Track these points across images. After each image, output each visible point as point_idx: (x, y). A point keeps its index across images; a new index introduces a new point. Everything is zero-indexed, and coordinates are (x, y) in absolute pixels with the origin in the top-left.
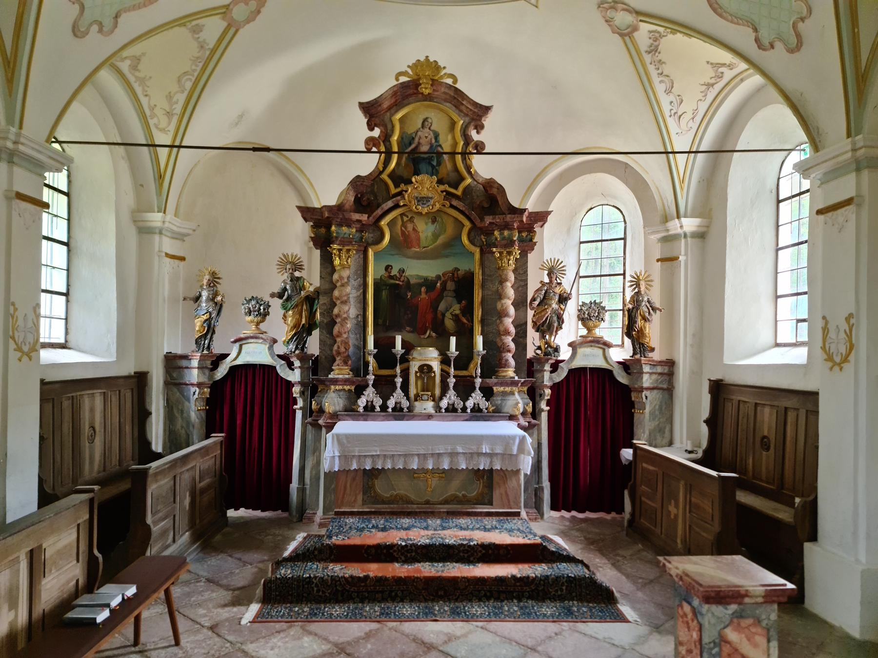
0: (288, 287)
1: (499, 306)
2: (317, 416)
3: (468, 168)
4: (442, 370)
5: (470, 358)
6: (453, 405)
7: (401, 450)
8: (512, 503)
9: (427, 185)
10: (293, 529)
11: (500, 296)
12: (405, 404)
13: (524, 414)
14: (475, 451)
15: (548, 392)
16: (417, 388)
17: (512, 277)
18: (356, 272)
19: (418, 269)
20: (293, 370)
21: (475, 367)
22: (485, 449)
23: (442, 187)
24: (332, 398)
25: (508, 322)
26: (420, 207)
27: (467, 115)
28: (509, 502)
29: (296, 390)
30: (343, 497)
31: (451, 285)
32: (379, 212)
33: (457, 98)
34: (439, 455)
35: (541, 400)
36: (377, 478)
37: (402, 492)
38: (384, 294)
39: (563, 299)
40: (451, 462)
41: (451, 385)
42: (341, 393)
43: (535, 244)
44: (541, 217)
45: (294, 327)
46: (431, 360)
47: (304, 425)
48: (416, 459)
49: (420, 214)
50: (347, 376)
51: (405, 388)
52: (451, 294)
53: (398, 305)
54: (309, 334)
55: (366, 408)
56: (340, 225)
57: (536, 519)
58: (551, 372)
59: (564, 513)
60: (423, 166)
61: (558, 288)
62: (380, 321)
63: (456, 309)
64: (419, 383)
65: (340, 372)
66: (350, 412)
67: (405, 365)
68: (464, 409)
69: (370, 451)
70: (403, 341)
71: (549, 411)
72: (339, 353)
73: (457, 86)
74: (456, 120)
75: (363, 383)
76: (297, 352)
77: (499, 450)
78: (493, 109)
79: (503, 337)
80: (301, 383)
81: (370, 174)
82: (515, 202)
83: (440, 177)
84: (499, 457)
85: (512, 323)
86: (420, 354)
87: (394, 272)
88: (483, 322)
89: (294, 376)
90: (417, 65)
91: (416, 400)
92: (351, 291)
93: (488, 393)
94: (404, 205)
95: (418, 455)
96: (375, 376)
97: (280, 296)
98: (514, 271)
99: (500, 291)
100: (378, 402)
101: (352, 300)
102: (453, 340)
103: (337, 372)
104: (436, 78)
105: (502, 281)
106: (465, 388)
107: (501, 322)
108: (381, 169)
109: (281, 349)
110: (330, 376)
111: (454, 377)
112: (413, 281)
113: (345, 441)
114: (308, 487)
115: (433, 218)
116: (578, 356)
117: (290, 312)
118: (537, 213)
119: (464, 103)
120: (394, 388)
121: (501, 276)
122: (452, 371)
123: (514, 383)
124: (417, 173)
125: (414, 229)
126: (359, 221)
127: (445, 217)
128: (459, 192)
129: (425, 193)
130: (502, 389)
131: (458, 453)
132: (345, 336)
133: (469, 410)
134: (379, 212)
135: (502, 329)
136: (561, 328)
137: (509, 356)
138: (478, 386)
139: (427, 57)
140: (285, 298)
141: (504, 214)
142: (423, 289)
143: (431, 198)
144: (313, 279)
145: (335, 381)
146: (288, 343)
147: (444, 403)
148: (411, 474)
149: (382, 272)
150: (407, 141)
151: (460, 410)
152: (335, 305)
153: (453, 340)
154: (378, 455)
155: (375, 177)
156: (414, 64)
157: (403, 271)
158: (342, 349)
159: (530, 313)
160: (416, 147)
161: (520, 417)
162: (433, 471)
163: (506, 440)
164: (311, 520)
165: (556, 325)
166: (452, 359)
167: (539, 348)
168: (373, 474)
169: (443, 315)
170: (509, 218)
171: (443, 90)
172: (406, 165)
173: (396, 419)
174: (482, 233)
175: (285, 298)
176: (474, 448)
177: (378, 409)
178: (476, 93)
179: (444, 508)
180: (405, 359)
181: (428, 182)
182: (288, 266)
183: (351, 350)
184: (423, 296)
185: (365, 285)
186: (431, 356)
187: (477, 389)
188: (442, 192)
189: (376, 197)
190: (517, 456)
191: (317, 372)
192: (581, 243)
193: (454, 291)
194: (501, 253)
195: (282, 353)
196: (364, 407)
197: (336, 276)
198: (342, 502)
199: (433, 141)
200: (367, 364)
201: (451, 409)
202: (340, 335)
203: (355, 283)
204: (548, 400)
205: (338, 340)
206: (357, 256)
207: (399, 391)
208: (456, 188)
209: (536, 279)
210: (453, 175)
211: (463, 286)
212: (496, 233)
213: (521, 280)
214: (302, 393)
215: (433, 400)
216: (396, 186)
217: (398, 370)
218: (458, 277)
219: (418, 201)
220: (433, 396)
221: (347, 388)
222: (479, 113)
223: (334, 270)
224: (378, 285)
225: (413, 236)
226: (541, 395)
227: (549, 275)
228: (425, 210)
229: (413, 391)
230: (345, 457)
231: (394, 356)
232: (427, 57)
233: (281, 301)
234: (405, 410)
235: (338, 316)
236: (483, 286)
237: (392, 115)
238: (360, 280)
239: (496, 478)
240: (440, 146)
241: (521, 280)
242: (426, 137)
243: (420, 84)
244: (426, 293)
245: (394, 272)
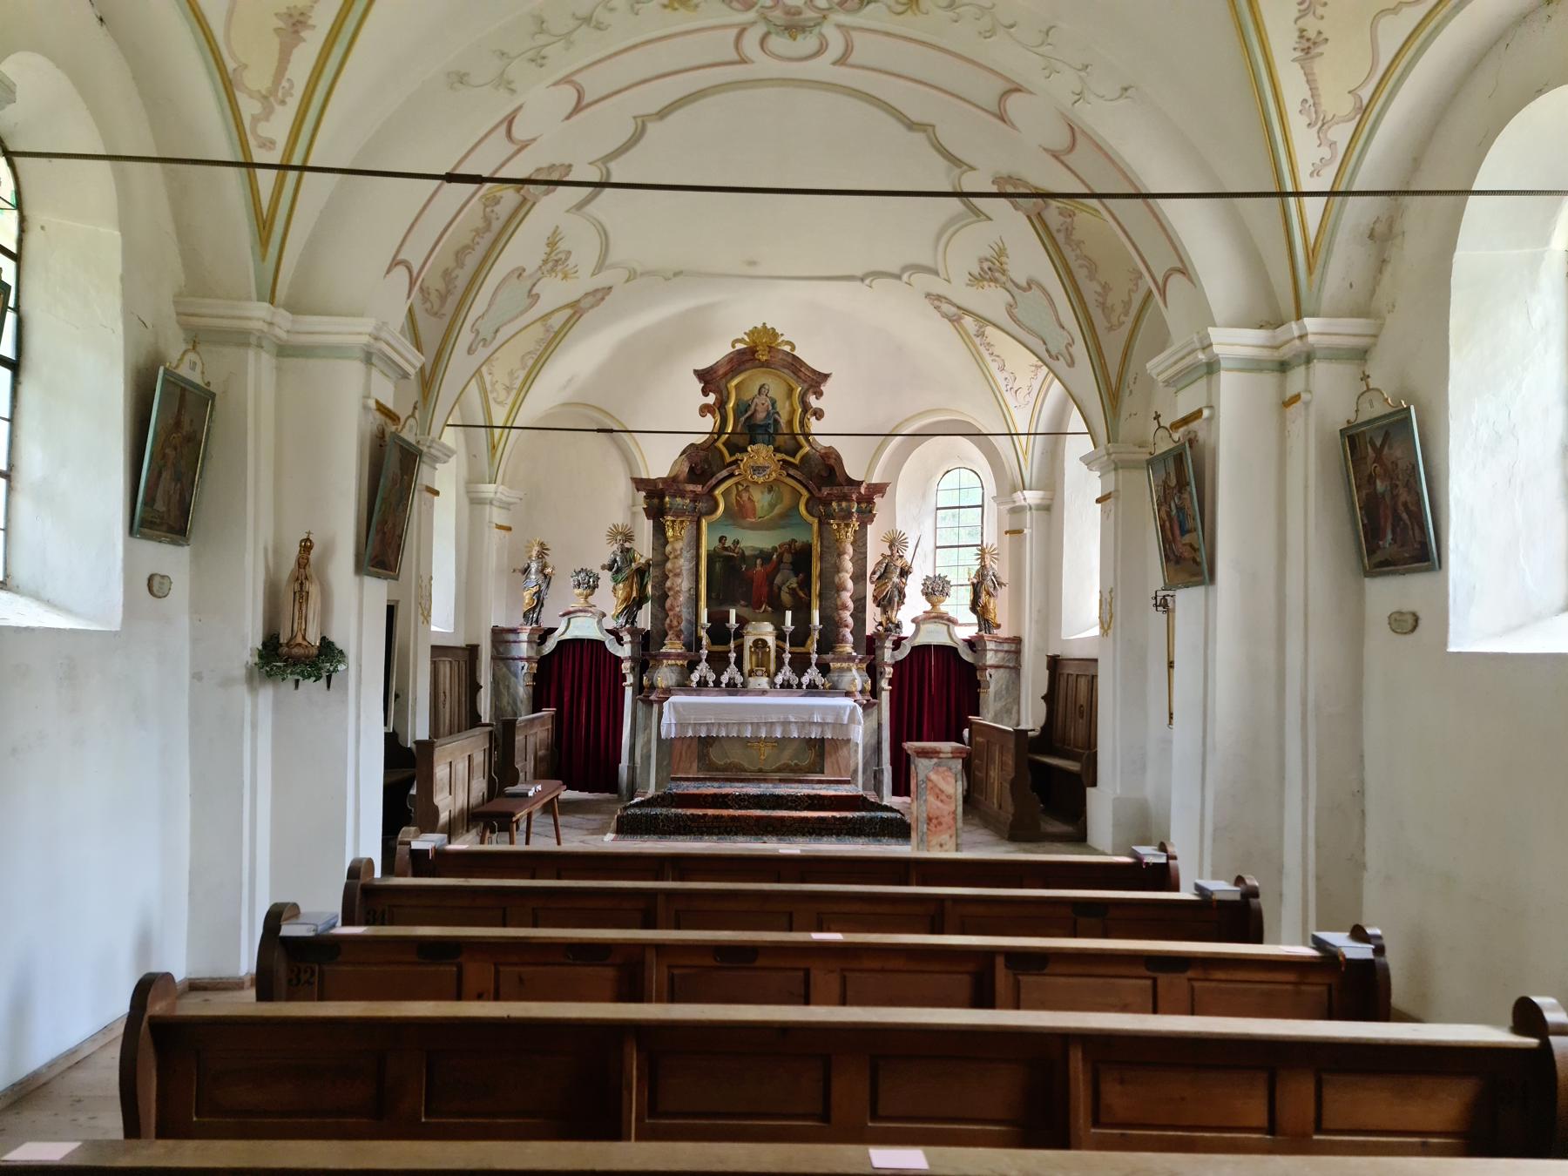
5: (808, 633)
7: (734, 718)
11: (838, 569)
12: (739, 679)
13: (862, 692)
15: (889, 670)
17: (850, 549)
19: (753, 541)
22: (817, 718)
25: (846, 597)
29: (626, 667)
31: (787, 558)
32: (713, 481)
33: (795, 365)
34: (772, 723)
39: (905, 573)
44: (880, 489)
51: (739, 663)
53: (731, 578)
54: (640, 608)
55: (698, 683)
56: (674, 496)
63: (793, 582)
65: (673, 646)
66: (683, 686)
68: (800, 685)
72: (671, 627)
77: (830, 720)
87: (728, 543)
88: (821, 596)
89: (624, 651)
90: (753, 333)
92: (684, 564)
93: (824, 669)
100: (711, 677)
102: (789, 614)
105: (840, 554)
109: (610, 623)
112: (747, 553)
123: (850, 659)
128: (796, 461)
129: (761, 462)
134: (713, 481)
137: (847, 632)
144: (644, 548)
145: (668, 656)
147: (779, 679)
153: (789, 614)
155: (709, 447)
168: (707, 742)
170: (846, 489)
176: (806, 718)
180: (739, 634)
183: (683, 625)
184: (759, 568)
185: (698, 557)
191: (648, 648)
197: (668, 548)
208: (794, 456)
209: (875, 552)
211: (800, 558)
216: (731, 455)
217: (732, 645)
220: (768, 672)
223: (666, 542)
225: (749, 505)
229: (747, 667)
230: (681, 725)
245: (728, 543)
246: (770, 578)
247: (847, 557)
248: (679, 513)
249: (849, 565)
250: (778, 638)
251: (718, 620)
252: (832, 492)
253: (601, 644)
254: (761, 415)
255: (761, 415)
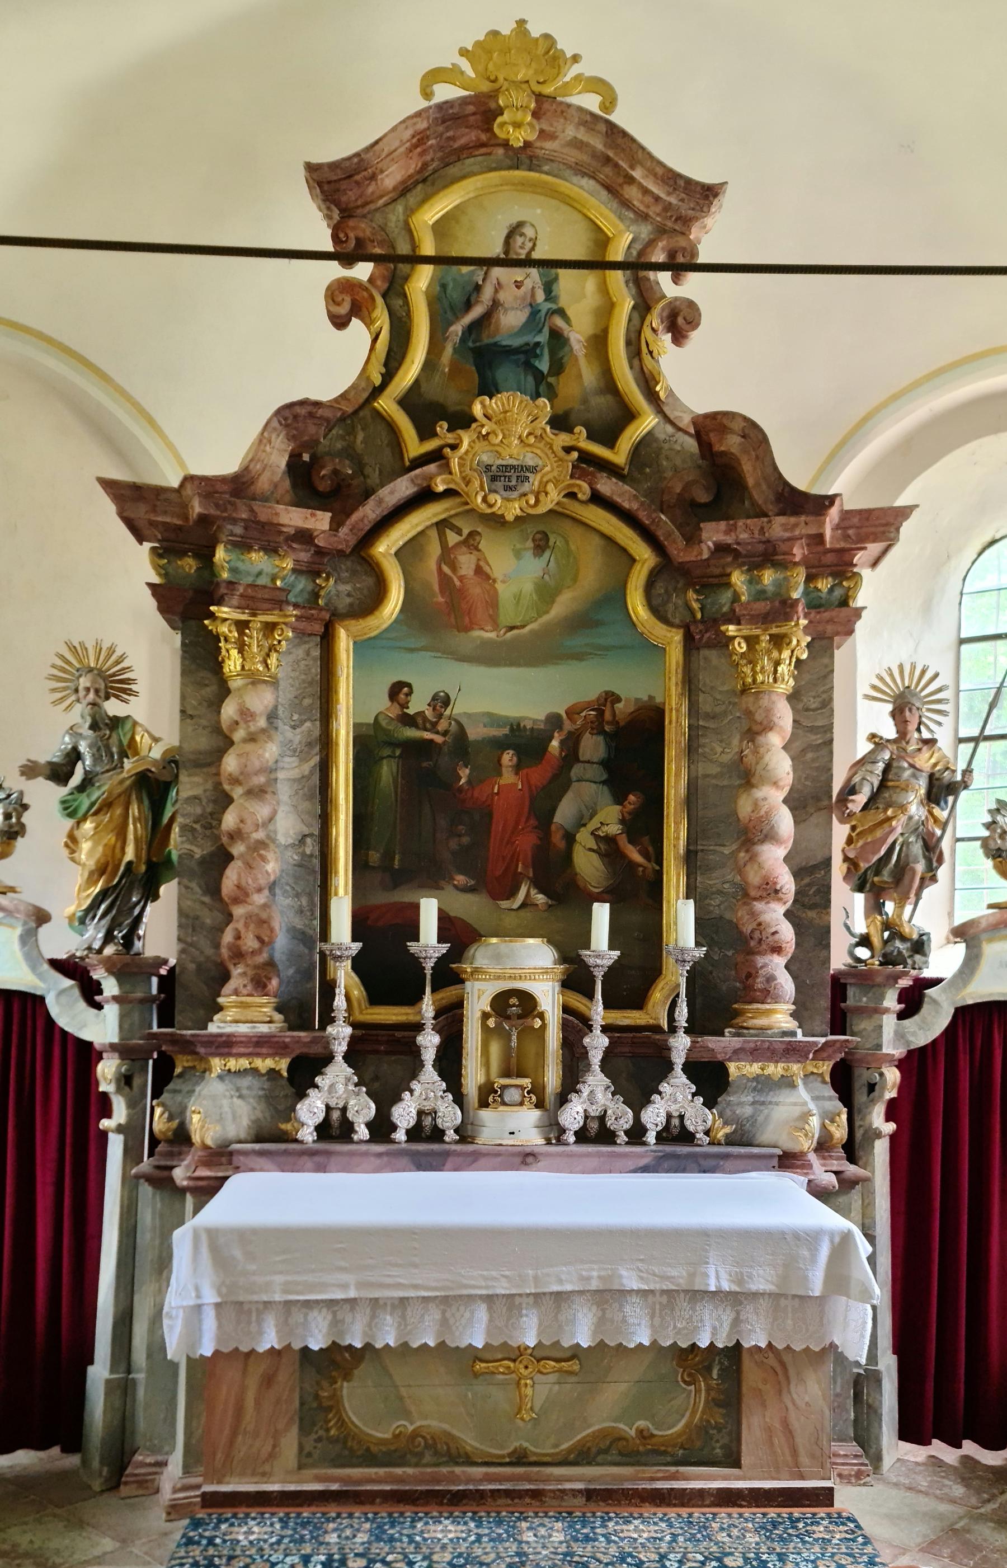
0: (83, 747)
1: (744, 808)
2: (170, 1155)
3: (648, 383)
4: (566, 1009)
5: (653, 972)
6: (602, 1118)
7: (425, 1279)
8: (804, 1459)
9: (522, 428)
10: (81, 1524)
11: (746, 776)
12: (449, 1116)
13: (823, 1147)
14: (683, 1283)
15: (893, 1076)
16: (487, 1064)
17: (784, 716)
18: (296, 704)
19: (491, 695)
20: (99, 1007)
21: (670, 996)
22: (717, 1277)
23: (564, 439)
24: (213, 1098)
25: (774, 859)
26: (496, 498)
27: (644, 217)
28: (795, 1453)
29: (107, 1071)
30: (231, 1442)
31: (593, 747)
32: (369, 512)
33: (613, 157)
34: (560, 1297)
35: (873, 1102)
36: (347, 1376)
37: (434, 1424)
38: (387, 771)
39: (941, 790)
40: (601, 1323)
41: (596, 1057)
42: (246, 1082)
43: (858, 613)
44: (880, 526)
45: (101, 870)
46: (530, 977)
47: (130, 1182)
48: (482, 1314)
49: (496, 521)
50: (264, 1029)
51: (450, 1064)
52: (598, 773)
53: (426, 805)
54: (151, 894)
55: (323, 1130)
56: (243, 546)
57: (859, 1475)
58: (902, 1016)
59: (939, 1448)
60: (505, 372)
61: (926, 754)
62: (374, 857)
63: (610, 819)
64: (495, 1049)
65: (243, 1014)
66: (273, 1139)
67: (449, 994)
68: (637, 1134)
69: (323, 1287)
70: (444, 919)
71: (893, 1138)
72: (238, 955)
73: (616, 117)
74: (609, 230)
75: (317, 1049)
76: (109, 950)
77: (761, 1282)
78: (727, 201)
79: (759, 906)
80: (122, 1050)
81: (343, 396)
82: (798, 474)
83: (562, 407)
84: (764, 1303)
85: (787, 859)
86: (498, 957)
87: (418, 704)
88: (691, 858)
89: (100, 1027)
90: (489, 48)
91: (484, 1104)
92: (276, 756)
93: (710, 1080)
94: (449, 493)
95: (489, 1299)
96: (354, 1025)
97: (59, 773)
98: (793, 698)
99: (750, 758)
100: (362, 1111)
101: (284, 792)
102: (601, 914)
103: (230, 1014)
104: (548, 90)
105: (755, 730)
106: (639, 1067)
107: (753, 858)
108: (377, 380)
109: (61, 940)
110: (213, 1028)
111: (605, 1029)
112: (475, 733)
113: (237, 1253)
114: (140, 1376)
115: (540, 533)
116: (985, 966)
117: (88, 826)
118: (866, 515)
119: (637, 174)
120: (416, 1066)
121: (749, 714)
122: (598, 1013)
123: (792, 1051)
124: (488, 389)
125: (479, 571)
126: (304, 537)
127: (576, 534)
128: (620, 455)
129: (514, 453)
130: (754, 1069)
131: (624, 1293)
132: (259, 899)
133: (651, 1137)
134: (369, 512)
135: (754, 878)
136: (934, 879)
137: (777, 966)
138: (679, 1059)
139: (521, 23)
140: (76, 780)
141: (766, 515)
142: (508, 758)
143: (534, 470)
144: (155, 715)
145: (225, 1045)
146: (82, 921)
147: (573, 1115)
148: (466, 1362)
149: (381, 704)
150: (456, 295)
151: (622, 1138)
152: (226, 800)
153: (601, 914)
154: (352, 1302)
155: (357, 410)
156: (478, 44)
157: (446, 701)
158: (250, 942)
159: (840, 832)
160: (487, 316)
161: (812, 1157)
162: (540, 1355)
163: (788, 1244)
164: (148, 1486)
165: (920, 867)
166: (599, 974)
167: (865, 941)
168: (336, 1362)
169: (570, 838)
170: (778, 527)
171: (571, 132)
172: (455, 368)
173: (420, 1167)
174: (690, 584)
175: (76, 780)
176: (678, 1275)
177: (362, 1132)
178: (671, 137)
179: (577, 1478)
180: (448, 974)
181: (524, 419)
182: (84, 682)
183: (282, 942)
184: (508, 777)
185: (326, 743)
186: (532, 963)
187: (678, 1069)
188: (568, 450)
189: (360, 467)
190: (821, 1300)
191: (172, 1013)
192: (962, 641)
193: (605, 764)
194: (751, 641)
195: (61, 955)
196: (319, 1128)
197: (229, 710)
198: (229, 1457)
199: (540, 296)
200: (329, 989)
201: (596, 1133)
202: (242, 895)
203: (297, 737)
204: (891, 1102)
205: (238, 911)
206: (300, 652)
207: (429, 1074)
208: (610, 443)
209: (864, 722)
210: (602, 403)
211: (632, 749)
212: (738, 579)
213: (812, 730)
214: (125, 1081)
215: (539, 1105)
216: (425, 433)
217: (428, 1007)
218: (614, 722)
219: (494, 479)
220: (538, 1090)
221: (264, 1064)
222: (685, 210)
223: (224, 691)
224: (368, 746)
225: (476, 591)
226: (871, 1087)
227: (898, 714)
228: (513, 510)
229: (473, 1076)
230: (235, 1309)
231: (415, 963)
232: (521, 23)
233: (63, 791)
234: (450, 1135)
235: (236, 835)
236: (692, 749)
237: (410, 212)
238: (312, 728)
239: (751, 1375)
240: (561, 312)
241: (812, 730)
242: (518, 285)
243: (500, 112)
244: (518, 768)
245: (418, 704)
246: (542, 806)
247: (775, 740)
248: (261, 598)
249: (781, 764)
250: (567, 984)
251: (383, 936)
252: (733, 533)
253: (30, 1004)
254: (512, 320)
255: (512, 320)
